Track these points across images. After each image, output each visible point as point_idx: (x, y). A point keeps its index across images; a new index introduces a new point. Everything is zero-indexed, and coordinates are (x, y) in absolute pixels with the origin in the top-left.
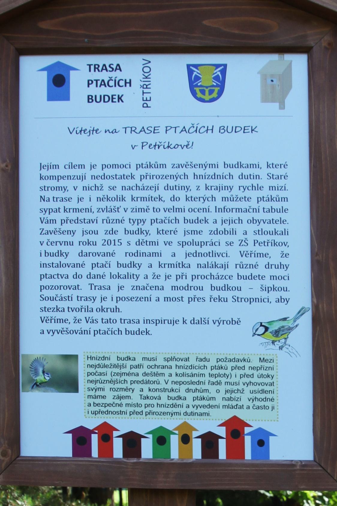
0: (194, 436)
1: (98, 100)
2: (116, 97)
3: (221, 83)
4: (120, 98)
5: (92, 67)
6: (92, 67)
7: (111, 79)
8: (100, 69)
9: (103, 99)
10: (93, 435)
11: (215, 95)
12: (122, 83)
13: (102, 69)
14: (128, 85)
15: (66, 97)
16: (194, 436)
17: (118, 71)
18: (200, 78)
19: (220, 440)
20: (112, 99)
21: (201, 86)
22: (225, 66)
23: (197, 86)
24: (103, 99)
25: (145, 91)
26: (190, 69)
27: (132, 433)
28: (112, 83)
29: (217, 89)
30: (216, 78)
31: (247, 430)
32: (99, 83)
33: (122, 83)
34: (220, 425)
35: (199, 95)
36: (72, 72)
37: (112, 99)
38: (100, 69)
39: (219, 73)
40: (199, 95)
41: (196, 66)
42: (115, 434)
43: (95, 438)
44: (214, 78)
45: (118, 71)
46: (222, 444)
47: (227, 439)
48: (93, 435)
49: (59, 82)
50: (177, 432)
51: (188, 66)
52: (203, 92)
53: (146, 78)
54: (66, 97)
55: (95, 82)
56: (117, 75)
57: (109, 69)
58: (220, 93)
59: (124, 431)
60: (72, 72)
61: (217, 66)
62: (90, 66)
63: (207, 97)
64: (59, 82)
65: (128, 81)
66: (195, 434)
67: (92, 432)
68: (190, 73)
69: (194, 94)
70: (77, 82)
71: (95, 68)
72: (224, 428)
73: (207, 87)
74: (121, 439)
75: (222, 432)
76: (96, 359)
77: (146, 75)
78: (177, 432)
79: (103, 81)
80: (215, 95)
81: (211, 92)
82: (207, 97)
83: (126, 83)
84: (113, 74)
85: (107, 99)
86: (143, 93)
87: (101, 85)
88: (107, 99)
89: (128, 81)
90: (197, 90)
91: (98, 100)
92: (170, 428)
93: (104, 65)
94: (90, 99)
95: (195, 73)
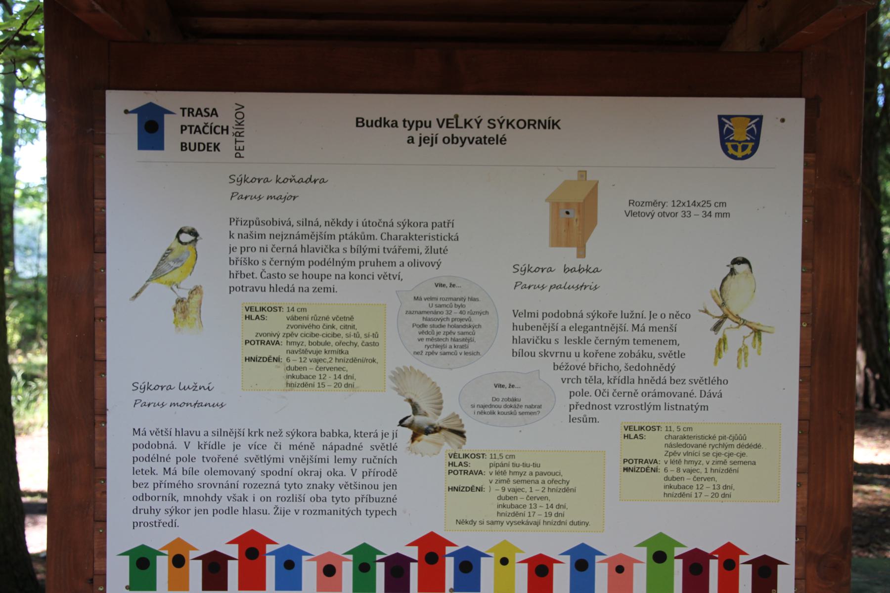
0: (191, 557)
1: (192, 148)
2: (212, 145)
3: (755, 136)
4: (216, 147)
5: (186, 111)
6: (186, 111)
7: (206, 125)
8: (195, 113)
10: (711, 561)
11: (748, 151)
12: (218, 130)
13: (197, 114)
14: (225, 132)
15: (160, 146)
16: (191, 557)
17: (214, 116)
18: (732, 132)
19: (230, 562)
20: (207, 147)
21: (733, 141)
22: (761, 117)
23: (728, 140)
24: (198, 147)
25: (238, 139)
26: (722, 120)
27: (765, 558)
28: (207, 130)
29: (751, 145)
30: (751, 132)
31: (269, 548)
32: (193, 129)
33: (218, 130)
36: (166, 116)
37: (207, 147)
38: (195, 113)
39: (753, 126)
41: (729, 117)
42: (742, 559)
43: (714, 566)
44: (748, 132)
45: (214, 116)
46: (233, 569)
48: (711, 561)
50: (166, 552)
51: (720, 117)
52: (735, 148)
53: (239, 124)
54: (160, 146)
55: (189, 128)
57: (204, 113)
59: (754, 554)
60: (166, 116)
61: (752, 118)
62: (183, 109)
63: (740, 154)
64: (151, 130)
65: (225, 128)
66: (193, 554)
67: (711, 556)
68: (721, 124)
69: (725, 149)
70: (171, 126)
71: (189, 112)
72: (415, 549)
73: (740, 142)
75: (233, 551)
77: (239, 121)
78: (166, 552)
79: (198, 126)
80: (748, 151)
81: (744, 148)
83: (223, 130)
84: (209, 120)
85: (202, 147)
86: (236, 141)
87: (195, 131)
88: (202, 147)
89: (225, 128)
90: (729, 145)
91: (192, 148)
92: (156, 547)
93: (199, 109)
94: (184, 147)
95: (727, 126)
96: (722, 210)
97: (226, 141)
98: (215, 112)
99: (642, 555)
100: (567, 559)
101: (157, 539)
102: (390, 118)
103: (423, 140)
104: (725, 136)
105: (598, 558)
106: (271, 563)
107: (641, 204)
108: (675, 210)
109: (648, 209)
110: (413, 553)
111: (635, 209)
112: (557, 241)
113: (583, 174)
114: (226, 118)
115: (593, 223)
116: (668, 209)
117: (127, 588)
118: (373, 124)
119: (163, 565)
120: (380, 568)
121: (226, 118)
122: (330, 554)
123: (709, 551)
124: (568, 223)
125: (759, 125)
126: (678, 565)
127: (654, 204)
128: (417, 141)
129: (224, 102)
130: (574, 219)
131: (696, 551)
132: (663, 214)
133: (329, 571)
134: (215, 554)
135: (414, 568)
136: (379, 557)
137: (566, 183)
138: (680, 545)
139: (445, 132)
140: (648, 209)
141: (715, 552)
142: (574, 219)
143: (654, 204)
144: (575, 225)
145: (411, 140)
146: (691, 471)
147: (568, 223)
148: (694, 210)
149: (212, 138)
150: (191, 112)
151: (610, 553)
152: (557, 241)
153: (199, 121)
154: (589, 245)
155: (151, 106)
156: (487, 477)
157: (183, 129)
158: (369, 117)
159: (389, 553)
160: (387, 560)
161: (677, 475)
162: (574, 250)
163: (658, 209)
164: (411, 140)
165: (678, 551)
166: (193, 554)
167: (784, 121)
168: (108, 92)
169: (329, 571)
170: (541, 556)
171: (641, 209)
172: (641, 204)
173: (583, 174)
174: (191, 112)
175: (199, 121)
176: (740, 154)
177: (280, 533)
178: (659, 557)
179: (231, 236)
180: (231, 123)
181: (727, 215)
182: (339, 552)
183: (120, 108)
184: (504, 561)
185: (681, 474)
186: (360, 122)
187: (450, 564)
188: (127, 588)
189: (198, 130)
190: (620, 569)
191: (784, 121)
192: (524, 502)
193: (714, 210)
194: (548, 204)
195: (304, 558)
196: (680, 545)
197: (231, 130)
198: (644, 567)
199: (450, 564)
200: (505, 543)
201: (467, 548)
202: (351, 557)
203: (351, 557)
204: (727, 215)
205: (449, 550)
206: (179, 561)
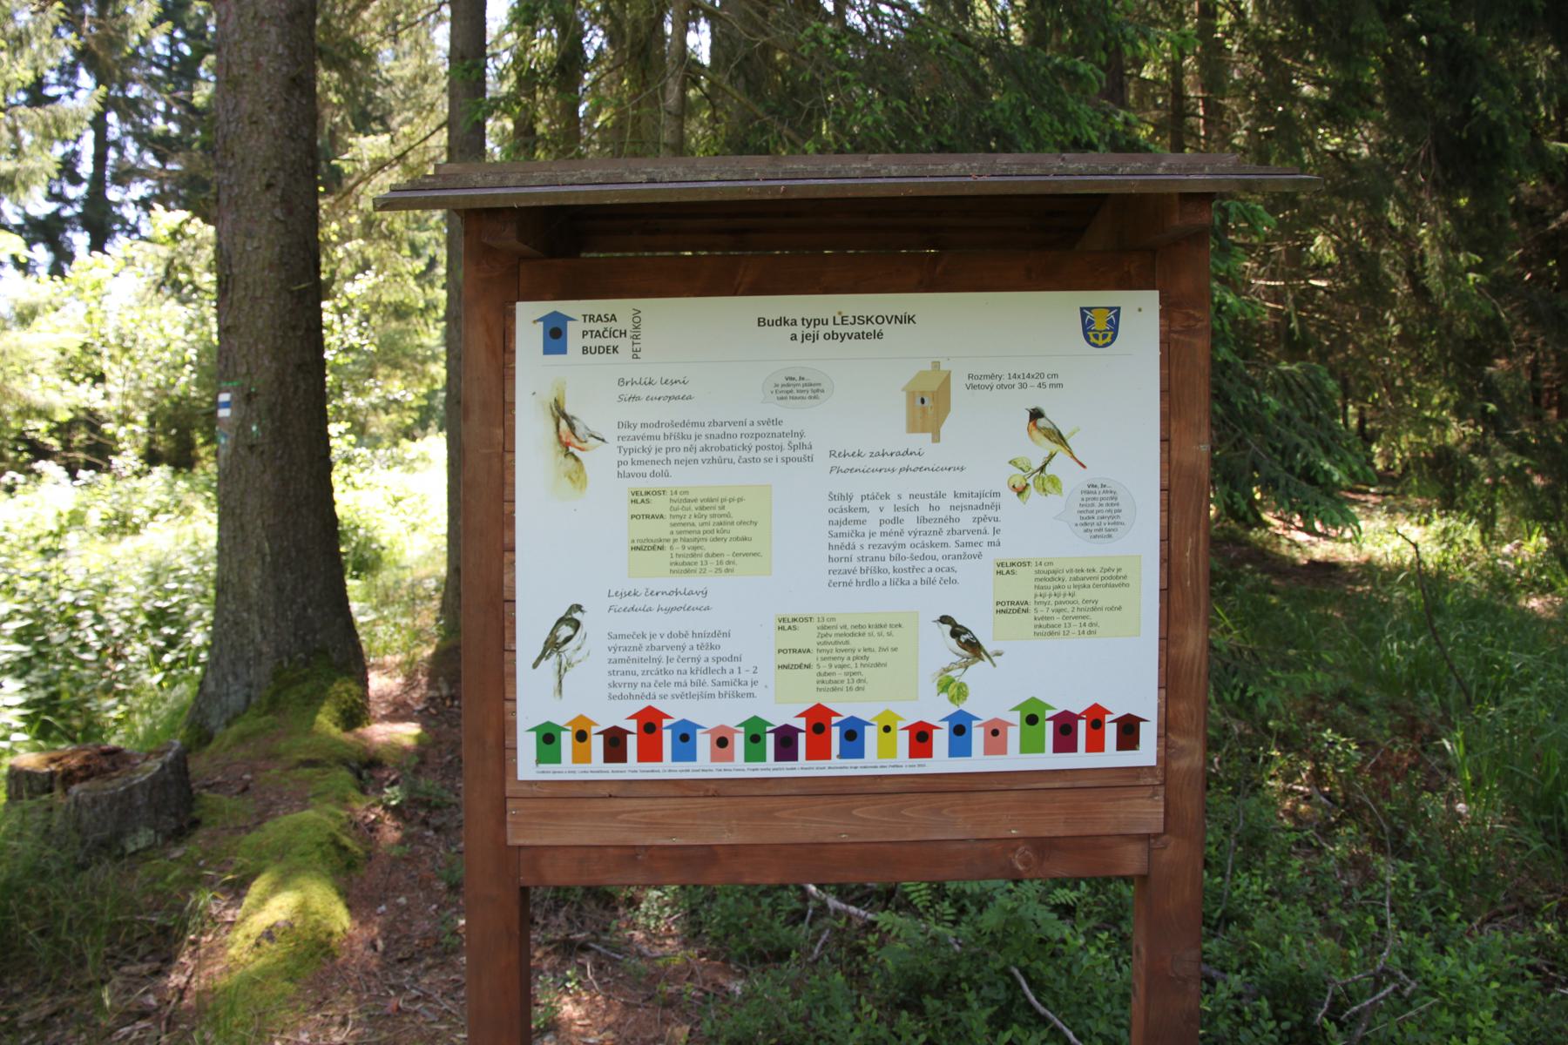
3: (1114, 326)
4: (615, 349)
11: (1108, 340)
22: (1117, 311)
27: (1129, 716)
30: (1110, 322)
31: (666, 722)
34: (800, 715)
35: (1093, 340)
40: (1093, 340)
41: (1090, 309)
42: (1108, 718)
43: (1082, 726)
46: (632, 743)
49: (555, 335)
52: (1096, 337)
56: (612, 325)
58: (1114, 338)
61: (1111, 309)
63: (1101, 342)
64: (555, 335)
66: (594, 730)
68: (1083, 316)
69: (1087, 338)
70: (573, 332)
72: (634, 722)
74: (1115, 725)
75: (632, 726)
76: (700, 635)
80: (1108, 340)
81: (1105, 337)
92: (561, 723)
94: (585, 350)
96: (1054, 381)
97: (624, 344)
98: (614, 318)
99: (1016, 718)
100: (946, 725)
101: (561, 715)
102: (789, 317)
104: (1087, 326)
105: (975, 723)
106: (667, 736)
110: (801, 724)
111: (976, 382)
112: (913, 427)
113: (936, 365)
114: (624, 323)
115: (947, 410)
116: (1005, 381)
118: (774, 323)
119: (567, 739)
120: (770, 740)
121: (624, 323)
122: (722, 727)
124: (924, 411)
125: (1117, 315)
126: (1050, 726)
128: (799, 337)
129: (622, 308)
130: (929, 407)
131: (1066, 713)
132: (1001, 386)
133: (722, 742)
134: (786, 727)
135: (802, 738)
136: (769, 729)
137: (922, 374)
138: (1051, 708)
141: (569, 724)
142: (929, 407)
144: (930, 412)
145: (794, 337)
147: (924, 411)
149: (611, 342)
150: (591, 318)
151: (986, 718)
152: (913, 427)
153: (600, 326)
154: (944, 430)
155: (555, 314)
156: (815, 654)
157: (584, 334)
158: (770, 317)
159: (778, 724)
160: (605, 733)
162: (929, 436)
163: (996, 382)
164: (794, 337)
165: (1049, 714)
166: (594, 730)
167: (1141, 312)
168: (519, 305)
169: (722, 742)
170: (921, 723)
173: (936, 365)
174: (591, 318)
175: (600, 326)
176: (1101, 342)
177: (676, 710)
178: (1032, 720)
180: (629, 327)
181: (1061, 385)
183: (529, 317)
184: (887, 729)
186: (761, 322)
187: (836, 733)
190: (685, 738)
191: (1141, 312)
192: (843, 677)
193: (1048, 382)
194: (904, 394)
196: (1051, 708)
199: (836, 733)
200: (887, 712)
204: (1061, 385)
205: (835, 720)
206: (581, 736)
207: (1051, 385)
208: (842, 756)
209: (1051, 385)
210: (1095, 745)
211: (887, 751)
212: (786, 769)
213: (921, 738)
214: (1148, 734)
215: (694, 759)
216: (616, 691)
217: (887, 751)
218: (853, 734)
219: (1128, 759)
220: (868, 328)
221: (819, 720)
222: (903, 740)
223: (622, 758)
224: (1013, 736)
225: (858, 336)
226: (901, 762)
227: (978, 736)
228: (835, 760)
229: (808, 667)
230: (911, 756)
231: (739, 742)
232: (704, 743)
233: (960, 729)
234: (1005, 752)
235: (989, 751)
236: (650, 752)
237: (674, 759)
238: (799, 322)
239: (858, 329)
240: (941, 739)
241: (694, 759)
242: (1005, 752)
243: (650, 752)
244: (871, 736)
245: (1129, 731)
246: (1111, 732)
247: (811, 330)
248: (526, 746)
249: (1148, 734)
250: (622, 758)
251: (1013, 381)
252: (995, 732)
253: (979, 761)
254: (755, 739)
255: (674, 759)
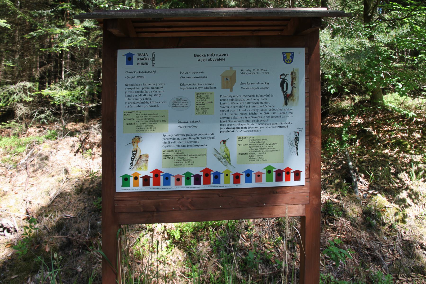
3: (292, 58)
4: (147, 64)
9: (142, 64)
11: (291, 62)
15: (132, 64)
24: (142, 64)
27: (297, 171)
30: (291, 57)
31: (161, 174)
35: (286, 62)
36: (134, 56)
40: (286, 62)
41: (285, 53)
42: (291, 171)
43: (284, 173)
46: (151, 180)
47: (153, 177)
49: (129, 59)
52: (287, 61)
54: (132, 64)
56: (146, 57)
61: (291, 53)
64: (129, 59)
66: (140, 176)
67: (283, 171)
68: (283, 55)
69: (284, 61)
70: (135, 59)
72: (152, 174)
74: (255, 175)
80: (291, 62)
81: (289, 61)
82: (288, 62)
84: (145, 57)
94: (138, 64)
96: (267, 72)
97: (150, 62)
98: (147, 54)
99: (265, 171)
102: (203, 54)
103: (203, 60)
104: (284, 58)
106: (162, 178)
107: (245, 71)
108: (254, 72)
109: (247, 72)
110: (202, 174)
111: (243, 72)
113: (231, 68)
114: (150, 56)
116: (252, 72)
117: (122, 186)
119: (132, 180)
120: (192, 178)
123: (282, 170)
125: (293, 55)
126: (274, 173)
127: (248, 70)
128: (201, 60)
132: (251, 73)
135: (202, 178)
136: (192, 175)
139: (209, 57)
140: (247, 72)
141: (285, 169)
143: (248, 70)
145: (199, 60)
146: (144, 124)
148: (259, 72)
149: (146, 61)
150: (140, 54)
151: (256, 171)
153: (142, 57)
155: (129, 54)
157: (138, 59)
158: (198, 54)
161: (140, 125)
163: (249, 72)
165: (274, 170)
166: (140, 176)
170: (237, 173)
171: (245, 72)
172: (245, 71)
173: (231, 68)
174: (140, 54)
175: (142, 57)
176: (288, 62)
178: (269, 172)
179: (221, 104)
180: (151, 57)
181: (268, 73)
182: (181, 174)
183: (121, 54)
185: (141, 125)
186: (195, 55)
187: (212, 176)
188: (122, 186)
189: (142, 59)
190: (259, 176)
193: (265, 72)
195: (171, 176)
197: (151, 59)
198: (265, 175)
199: (212, 176)
201: (217, 172)
202: (184, 175)
203: (184, 175)
204: (268, 73)
205: (212, 172)
206: (136, 178)
207: (266, 73)
208: (213, 183)
209: (266, 73)
210: (288, 179)
211: (227, 182)
212: (297, 183)
213: (237, 178)
214: (303, 176)
215: (219, 183)
216: (176, 164)
217: (227, 182)
218: (217, 176)
219: (297, 183)
220: (221, 57)
221: (207, 172)
222: (232, 178)
223: (148, 185)
224: (264, 177)
225: (218, 60)
226: (232, 185)
227: (254, 177)
228: (212, 185)
229: (246, 154)
230: (143, 186)
231: (183, 179)
232: (173, 180)
233: (248, 174)
234: (261, 182)
235: (295, 179)
236: (157, 183)
237: (164, 185)
238: (206, 55)
239: (218, 57)
240: (243, 178)
241: (219, 183)
242: (261, 182)
243: (207, 182)
244: (222, 177)
245: (297, 175)
246: (292, 175)
247: (202, 58)
248: (119, 182)
249: (303, 176)
250: (148, 185)
251: (254, 72)
252: (259, 175)
253: (254, 184)
254: (188, 178)
255: (164, 185)
